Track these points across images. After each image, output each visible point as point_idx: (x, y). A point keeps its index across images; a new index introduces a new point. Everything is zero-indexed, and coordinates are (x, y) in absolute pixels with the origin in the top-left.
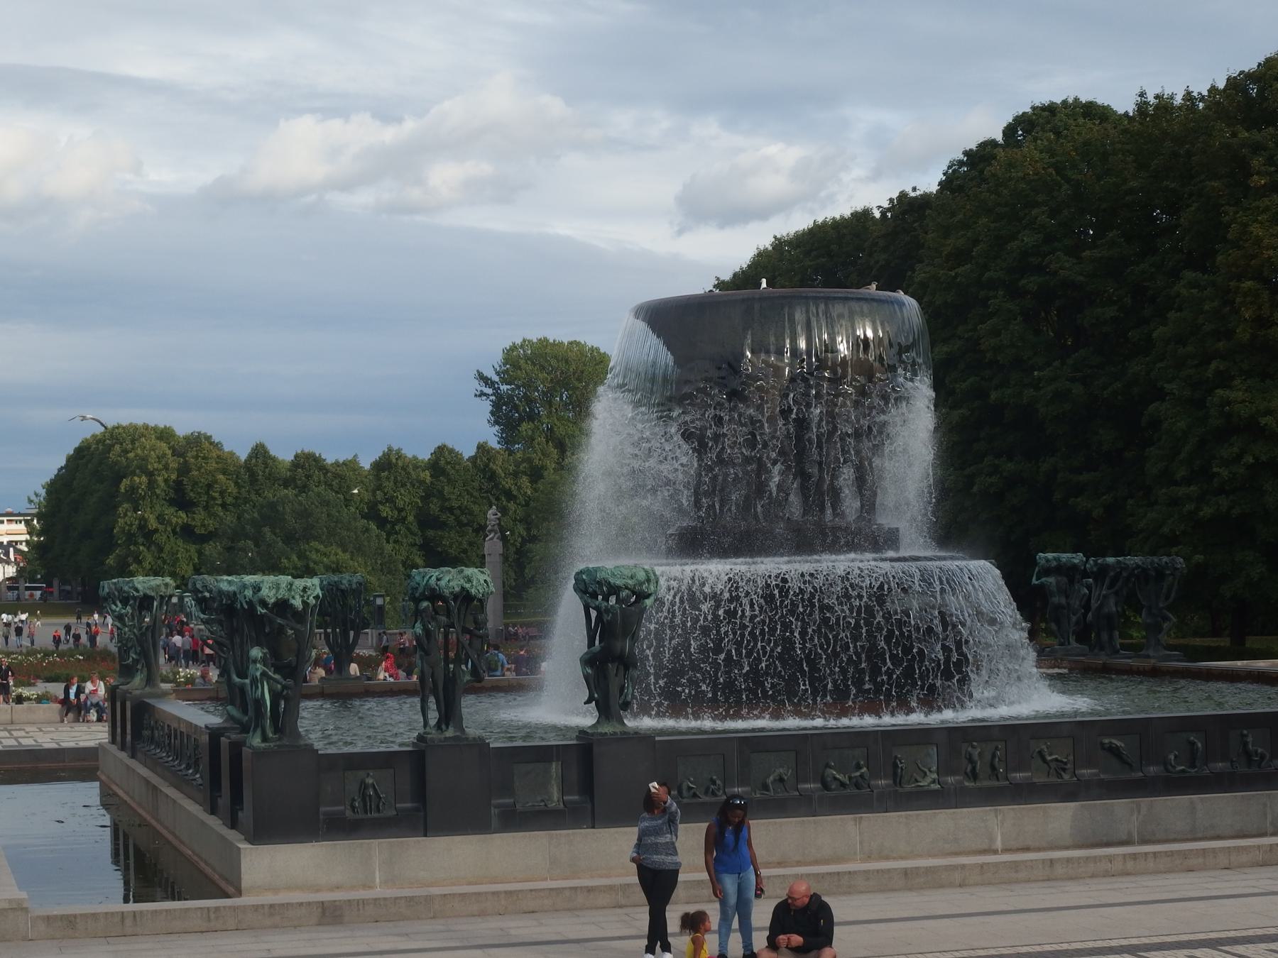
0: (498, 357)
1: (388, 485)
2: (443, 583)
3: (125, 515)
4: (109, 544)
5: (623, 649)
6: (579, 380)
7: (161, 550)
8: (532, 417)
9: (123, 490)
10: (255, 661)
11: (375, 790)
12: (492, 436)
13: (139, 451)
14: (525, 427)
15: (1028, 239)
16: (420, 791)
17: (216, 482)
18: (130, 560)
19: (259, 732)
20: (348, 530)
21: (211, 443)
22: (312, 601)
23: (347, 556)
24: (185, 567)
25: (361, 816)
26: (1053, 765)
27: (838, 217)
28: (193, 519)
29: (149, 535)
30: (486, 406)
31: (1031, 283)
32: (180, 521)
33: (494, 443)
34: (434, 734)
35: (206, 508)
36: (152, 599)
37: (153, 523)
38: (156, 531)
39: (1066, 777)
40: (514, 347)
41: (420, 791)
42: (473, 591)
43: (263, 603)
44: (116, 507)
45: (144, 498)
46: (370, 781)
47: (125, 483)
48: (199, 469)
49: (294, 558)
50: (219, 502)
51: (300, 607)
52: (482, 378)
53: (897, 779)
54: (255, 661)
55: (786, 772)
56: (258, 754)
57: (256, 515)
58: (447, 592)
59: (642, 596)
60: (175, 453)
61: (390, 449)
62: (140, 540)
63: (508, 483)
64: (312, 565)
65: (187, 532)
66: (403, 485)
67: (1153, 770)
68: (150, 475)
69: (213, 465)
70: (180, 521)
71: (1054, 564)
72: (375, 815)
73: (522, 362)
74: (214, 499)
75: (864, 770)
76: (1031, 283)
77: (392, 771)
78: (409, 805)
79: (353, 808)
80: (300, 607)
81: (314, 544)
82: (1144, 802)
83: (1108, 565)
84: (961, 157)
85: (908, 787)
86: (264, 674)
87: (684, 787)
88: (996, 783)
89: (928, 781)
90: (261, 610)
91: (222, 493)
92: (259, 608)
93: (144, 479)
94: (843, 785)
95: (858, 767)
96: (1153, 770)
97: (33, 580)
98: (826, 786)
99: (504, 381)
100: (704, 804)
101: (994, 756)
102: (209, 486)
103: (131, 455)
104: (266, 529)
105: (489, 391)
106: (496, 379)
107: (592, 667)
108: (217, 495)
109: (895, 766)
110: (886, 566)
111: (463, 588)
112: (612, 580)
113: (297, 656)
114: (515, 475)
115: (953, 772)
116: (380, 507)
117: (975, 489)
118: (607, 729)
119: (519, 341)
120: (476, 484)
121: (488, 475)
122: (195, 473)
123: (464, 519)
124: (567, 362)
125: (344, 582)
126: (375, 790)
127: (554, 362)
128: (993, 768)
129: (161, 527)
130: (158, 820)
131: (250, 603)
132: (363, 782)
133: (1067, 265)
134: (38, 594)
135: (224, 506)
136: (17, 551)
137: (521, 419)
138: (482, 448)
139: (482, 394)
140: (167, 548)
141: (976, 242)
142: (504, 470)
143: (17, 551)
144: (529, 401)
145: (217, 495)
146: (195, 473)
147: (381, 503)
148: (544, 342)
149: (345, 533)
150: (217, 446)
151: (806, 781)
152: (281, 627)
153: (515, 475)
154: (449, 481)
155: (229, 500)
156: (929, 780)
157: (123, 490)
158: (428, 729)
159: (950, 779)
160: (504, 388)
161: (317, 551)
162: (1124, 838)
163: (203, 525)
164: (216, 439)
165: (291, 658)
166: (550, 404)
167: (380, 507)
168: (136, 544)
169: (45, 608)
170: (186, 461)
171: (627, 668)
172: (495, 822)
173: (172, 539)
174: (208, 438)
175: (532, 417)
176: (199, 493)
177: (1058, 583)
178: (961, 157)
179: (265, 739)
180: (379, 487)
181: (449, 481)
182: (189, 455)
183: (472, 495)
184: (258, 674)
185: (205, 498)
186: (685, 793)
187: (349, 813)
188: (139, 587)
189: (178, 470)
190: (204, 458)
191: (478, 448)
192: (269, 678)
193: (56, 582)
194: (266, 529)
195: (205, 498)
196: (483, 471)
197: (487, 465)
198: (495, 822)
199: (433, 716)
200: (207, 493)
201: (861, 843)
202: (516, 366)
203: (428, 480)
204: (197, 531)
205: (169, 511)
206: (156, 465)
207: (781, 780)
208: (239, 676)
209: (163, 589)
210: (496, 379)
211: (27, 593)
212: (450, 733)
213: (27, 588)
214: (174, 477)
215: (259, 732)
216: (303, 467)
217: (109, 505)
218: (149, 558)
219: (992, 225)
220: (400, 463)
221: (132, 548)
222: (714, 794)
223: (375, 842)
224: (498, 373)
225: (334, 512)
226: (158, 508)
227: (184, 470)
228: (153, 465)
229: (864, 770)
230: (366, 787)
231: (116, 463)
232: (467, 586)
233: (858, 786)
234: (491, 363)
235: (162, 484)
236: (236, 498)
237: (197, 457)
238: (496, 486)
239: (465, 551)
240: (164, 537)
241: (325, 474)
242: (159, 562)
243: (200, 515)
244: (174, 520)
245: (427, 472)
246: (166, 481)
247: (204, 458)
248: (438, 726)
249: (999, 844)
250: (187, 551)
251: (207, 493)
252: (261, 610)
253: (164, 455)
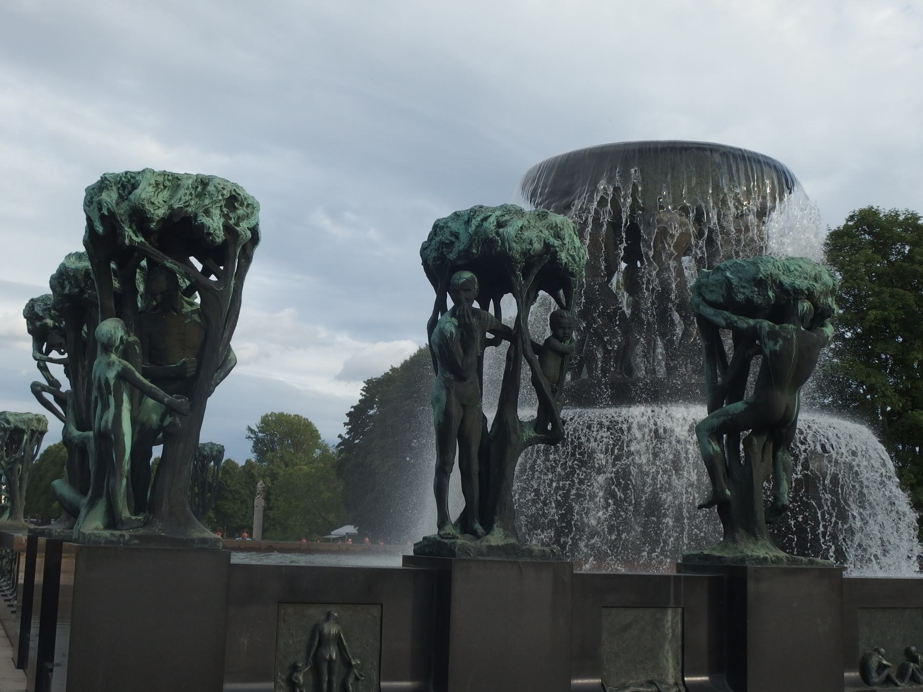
10: (108, 348)
11: (341, 649)
12: (253, 457)
14: (269, 455)
19: (101, 508)
30: (251, 443)
36: (22, 432)
40: (267, 416)
46: (332, 629)
51: (220, 236)
52: (250, 429)
54: (108, 348)
56: (91, 551)
77: (375, 611)
80: (220, 236)
86: (123, 376)
87: (874, 661)
90: (131, 236)
92: (129, 232)
99: (260, 431)
105: (253, 436)
106: (257, 430)
111: (547, 246)
112: (786, 280)
113: (200, 357)
119: (269, 413)
123: (236, 496)
126: (341, 649)
132: (316, 630)
137: (267, 451)
138: (248, 462)
139: (249, 437)
144: (273, 442)
148: (281, 415)
158: (449, 529)
160: (260, 435)
165: (183, 360)
166: (282, 444)
175: (273, 450)
179: (112, 521)
184: (111, 375)
199: (456, 504)
208: (79, 429)
209: (35, 423)
210: (257, 430)
212: (497, 538)
215: (101, 508)
234: (255, 423)
239: (236, 512)
248: (464, 522)
252: (131, 236)
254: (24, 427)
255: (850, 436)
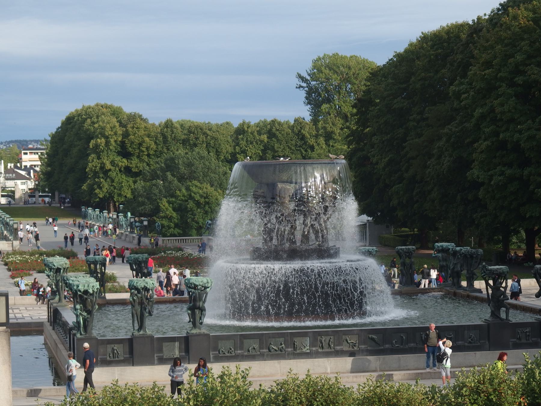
0: (309, 66)
1: (243, 143)
2: (138, 284)
3: (93, 161)
4: (83, 177)
5: (199, 305)
6: (356, 78)
7: (113, 181)
8: (328, 100)
9: (91, 147)
12: (305, 113)
13: (101, 123)
15: (519, 57)
16: (131, 352)
17: (144, 142)
18: (95, 186)
20: (215, 173)
21: (142, 119)
22: (96, 290)
23: (213, 189)
24: (126, 191)
25: (112, 359)
26: (351, 344)
27: (454, 23)
28: (131, 163)
29: (106, 172)
30: (303, 94)
31: (519, 80)
32: (123, 164)
33: (308, 118)
34: (136, 333)
35: (138, 157)
36: (60, 269)
37: (108, 166)
38: (110, 170)
39: (355, 348)
41: (131, 352)
42: (148, 287)
43: (80, 291)
44: (88, 155)
45: (103, 151)
46: (115, 348)
47: (92, 143)
48: (134, 135)
49: (184, 191)
50: (146, 153)
53: (295, 348)
55: (256, 346)
57: (163, 165)
58: (139, 287)
59: (206, 288)
60: (121, 125)
61: (244, 123)
62: (101, 175)
63: (312, 141)
64: (193, 194)
65: (128, 171)
66: (252, 143)
67: (387, 346)
68: (107, 138)
69: (142, 132)
70: (123, 164)
71: (441, 248)
72: (117, 359)
73: (323, 68)
74: (143, 152)
75: (283, 345)
76: (519, 80)
78: (128, 356)
79: (110, 357)
81: (196, 182)
82: (382, 357)
83: (456, 251)
84: (498, 6)
85: (298, 351)
86: (80, 314)
88: (330, 350)
89: (306, 350)
91: (147, 148)
93: (103, 140)
94: (276, 350)
95: (281, 344)
96: (387, 346)
97: (44, 191)
98: (270, 351)
99: (313, 80)
100: (227, 356)
101: (330, 341)
102: (140, 144)
103: (96, 126)
104: (168, 173)
105: (304, 85)
106: (309, 78)
107: (190, 310)
108: (144, 149)
109: (294, 344)
110: (328, 265)
114: (317, 136)
115: (315, 347)
116: (238, 156)
117: (492, 183)
118: (194, 331)
120: (293, 142)
121: (300, 137)
122: (132, 137)
124: (350, 68)
125: (140, 258)
127: (341, 68)
128: (329, 345)
129: (112, 168)
130: (57, 355)
131: (76, 291)
132: (113, 348)
133: (536, 72)
134: (47, 199)
135: (149, 155)
136: (35, 171)
139: (300, 87)
140: (116, 180)
141: (495, 57)
142: (310, 134)
143: (35, 171)
145: (144, 149)
146: (132, 137)
147: (238, 153)
148: (335, 55)
149: (212, 175)
150: (145, 121)
151: (263, 349)
152: (86, 299)
153: (317, 136)
154: (278, 140)
155: (152, 152)
156: (306, 349)
157: (91, 147)
159: (314, 349)
161: (196, 186)
162: (374, 369)
163: (137, 167)
164: (144, 116)
165: (90, 308)
167: (238, 156)
168: (99, 177)
169: (51, 213)
170: (127, 130)
171: (202, 311)
172: (156, 362)
173: (119, 175)
174: (140, 116)
176: (134, 148)
177: (442, 256)
178: (498, 6)
179: (81, 334)
180: (238, 144)
181: (278, 140)
182: (129, 126)
183: (291, 149)
185: (138, 151)
186: (221, 352)
187: (108, 358)
188: (55, 265)
189: (123, 135)
190: (137, 128)
191: (295, 121)
192: (82, 315)
193: (57, 193)
194: (168, 173)
195: (138, 151)
196: (298, 135)
197: (300, 131)
198: (156, 362)
200: (139, 148)
201: (280, 370)
202: (320, 71)
203: (266, 140)
204: (133, 170)
205: (118, 159)
206: (110, 133)
207: (254, 348)
209: (64, 265)
210: (309, 78)
211: (40, 199)
212: (141, 332)
213: (40, 196)
214: (120, 139)
216: (194, 133)
217: (84, 155)
218: (106, 186)
219: (503, 49)
220: (250, 131)
221: (97, 180)
222: (231, 353)
223: (116, 368)
224: (309, 75)
225: (207, 163)
226: (111, 157)
227: (126, 135)
228: (108, 132)
229: (283, 345)
230: (114, 350)
231: (88, 130)
232: (146, 285)
233: (281, 351)
234: (305, 67)
235: (113, 143)
236: (155, 151)
237: (133, 128)
238: (305, 143)
240: (115, 173)
241: (206, 137)
242: (112, 188)
243: (135, 161)
244: (120, 164)
245: (265, 136)
246: (115, 141)
247: (137, 128)
248: (139, 330)
249: (329, 371)
250: (128, 182)
251: (139, 148)
253: (115, 126)
254: (61, 267)
255: (374, 270)
